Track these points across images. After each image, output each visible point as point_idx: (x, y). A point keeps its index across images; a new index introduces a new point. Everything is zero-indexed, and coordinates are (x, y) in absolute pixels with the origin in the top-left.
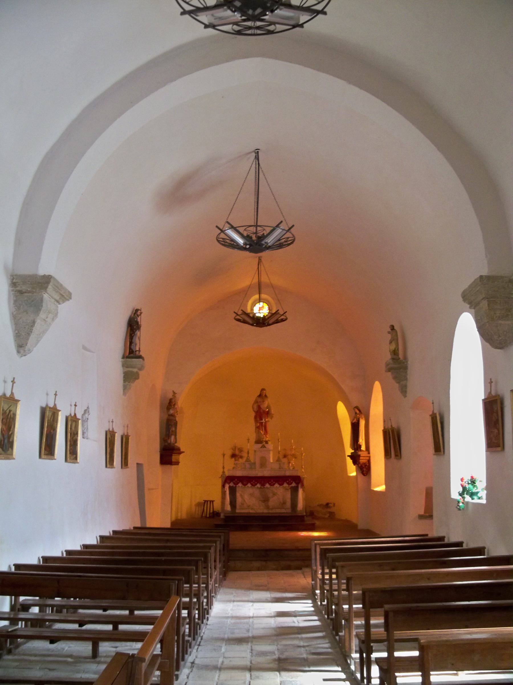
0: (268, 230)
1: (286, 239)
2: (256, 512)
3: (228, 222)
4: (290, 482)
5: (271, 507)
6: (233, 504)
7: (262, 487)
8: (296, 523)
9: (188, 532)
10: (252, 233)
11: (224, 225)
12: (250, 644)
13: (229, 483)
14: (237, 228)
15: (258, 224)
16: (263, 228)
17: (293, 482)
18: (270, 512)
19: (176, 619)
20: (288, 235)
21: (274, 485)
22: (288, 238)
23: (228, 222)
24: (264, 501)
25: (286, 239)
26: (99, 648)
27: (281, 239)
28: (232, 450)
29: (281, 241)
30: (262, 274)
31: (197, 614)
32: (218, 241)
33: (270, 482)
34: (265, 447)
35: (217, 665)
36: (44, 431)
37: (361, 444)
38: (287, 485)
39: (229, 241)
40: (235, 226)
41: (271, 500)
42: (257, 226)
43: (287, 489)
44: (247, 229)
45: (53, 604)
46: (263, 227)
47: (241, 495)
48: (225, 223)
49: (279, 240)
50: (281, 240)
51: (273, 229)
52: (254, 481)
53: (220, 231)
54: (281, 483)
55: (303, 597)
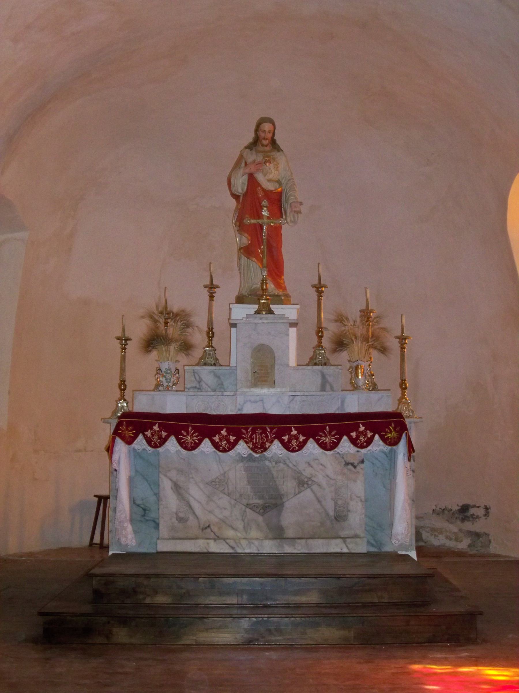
2: (231, 551)
4: (362, 438)
5: (290, 533)
7: (256, 455)
8: (285, 627)
9: (436, 669)
13: (129, 441)
17: (373, 437)
18: (288, 549)
19: (267, 603)
21: (301, 446)
24: (264, 509)
28: (148, 321)
30: (225, 573)
33: (286, 438)
34: (271, 312)
38: (353, 449)
41: (290, 504)
43: (352, 464)
47: (177, 487)
52: (224, 432)
54: (327, 440)
55: (103, 504)
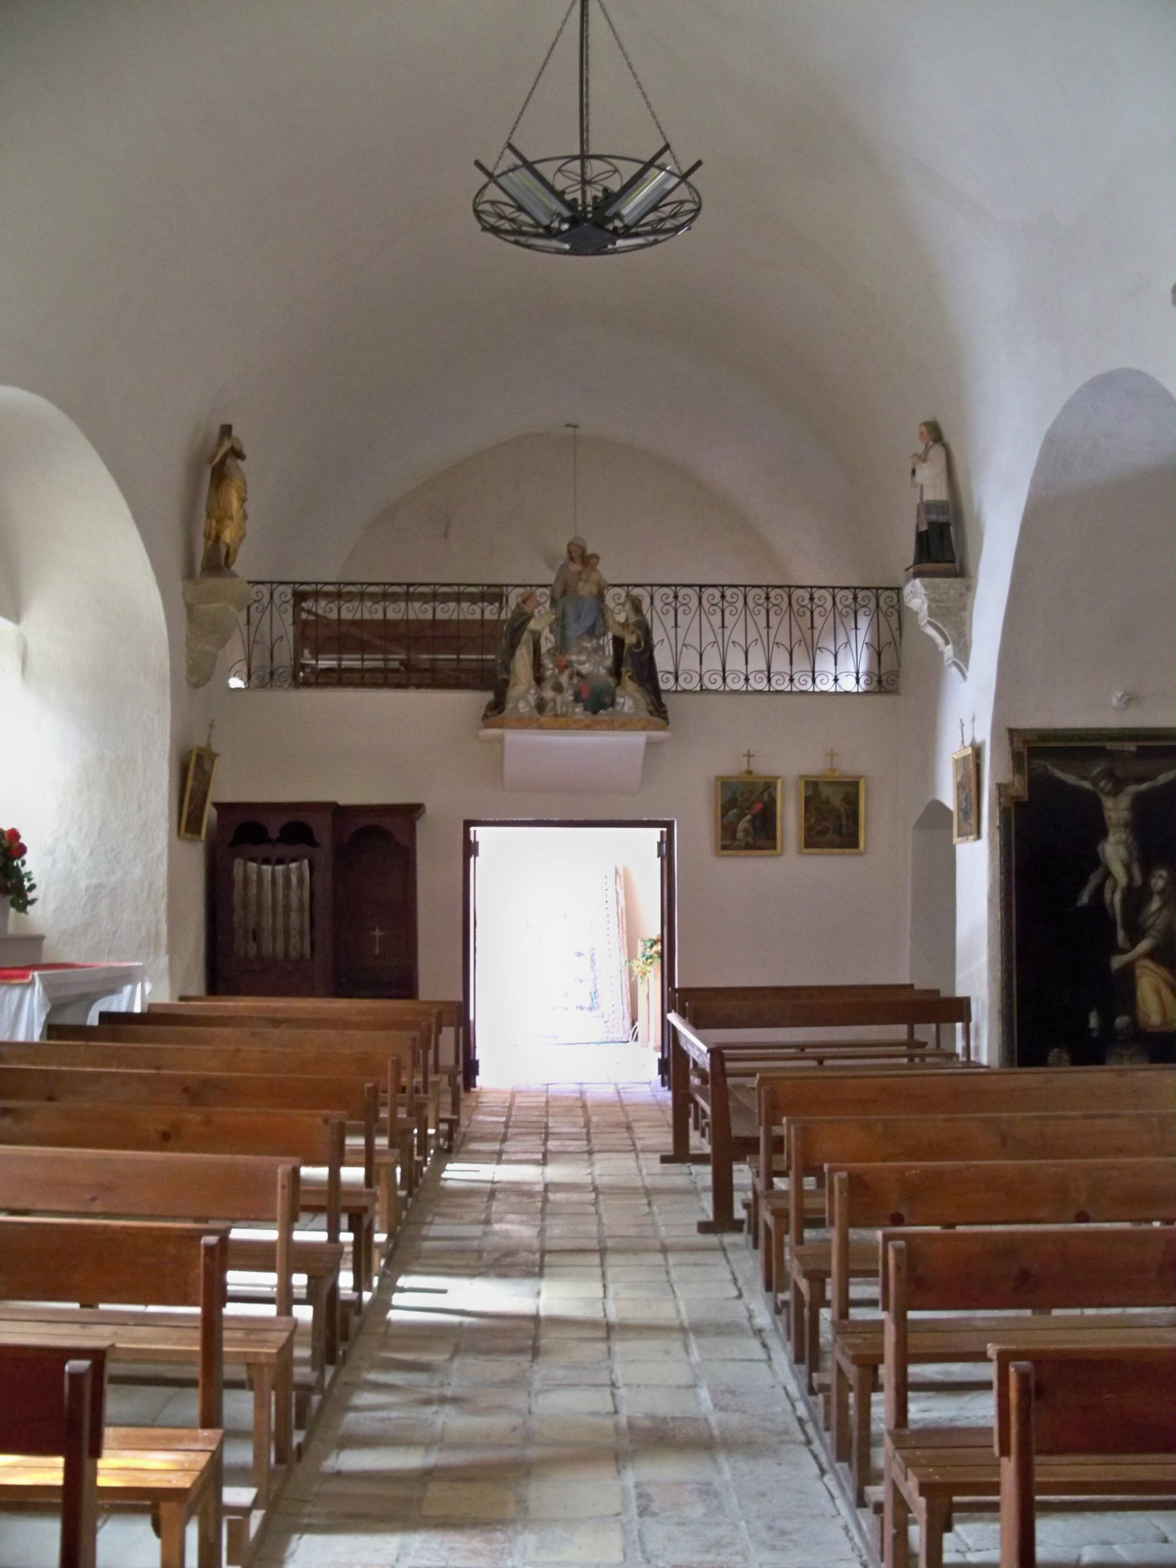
0: (629, 170)
1: (676, 205)
3: (510, 146)
6: (307, 1192)
10: (595, 182)
11: (502, 153)
12: (623, 1420)
14: (537, 166)
15: (577, 152)
16: (613, 166)
20: (682, 192)
22: (682, 202)
23: (510, 146)
25: (676, 205)
26: (222, 1369)
27: (661, 204)
29: (662, 212)
31: (911, 1032)
32: (478, 213)
35: (697, 1337)
36: (355, 667)
37: (703, 1066)
39: (512, 210)
40: (530, 159)
42: (584, 157)
44: (565, 168)
45: (860, 822)
46: (609, 160)
48: (505, 149)
49: (655, 208)
50: (661, 209)
51: (643, 168)
53: (486, 179)
